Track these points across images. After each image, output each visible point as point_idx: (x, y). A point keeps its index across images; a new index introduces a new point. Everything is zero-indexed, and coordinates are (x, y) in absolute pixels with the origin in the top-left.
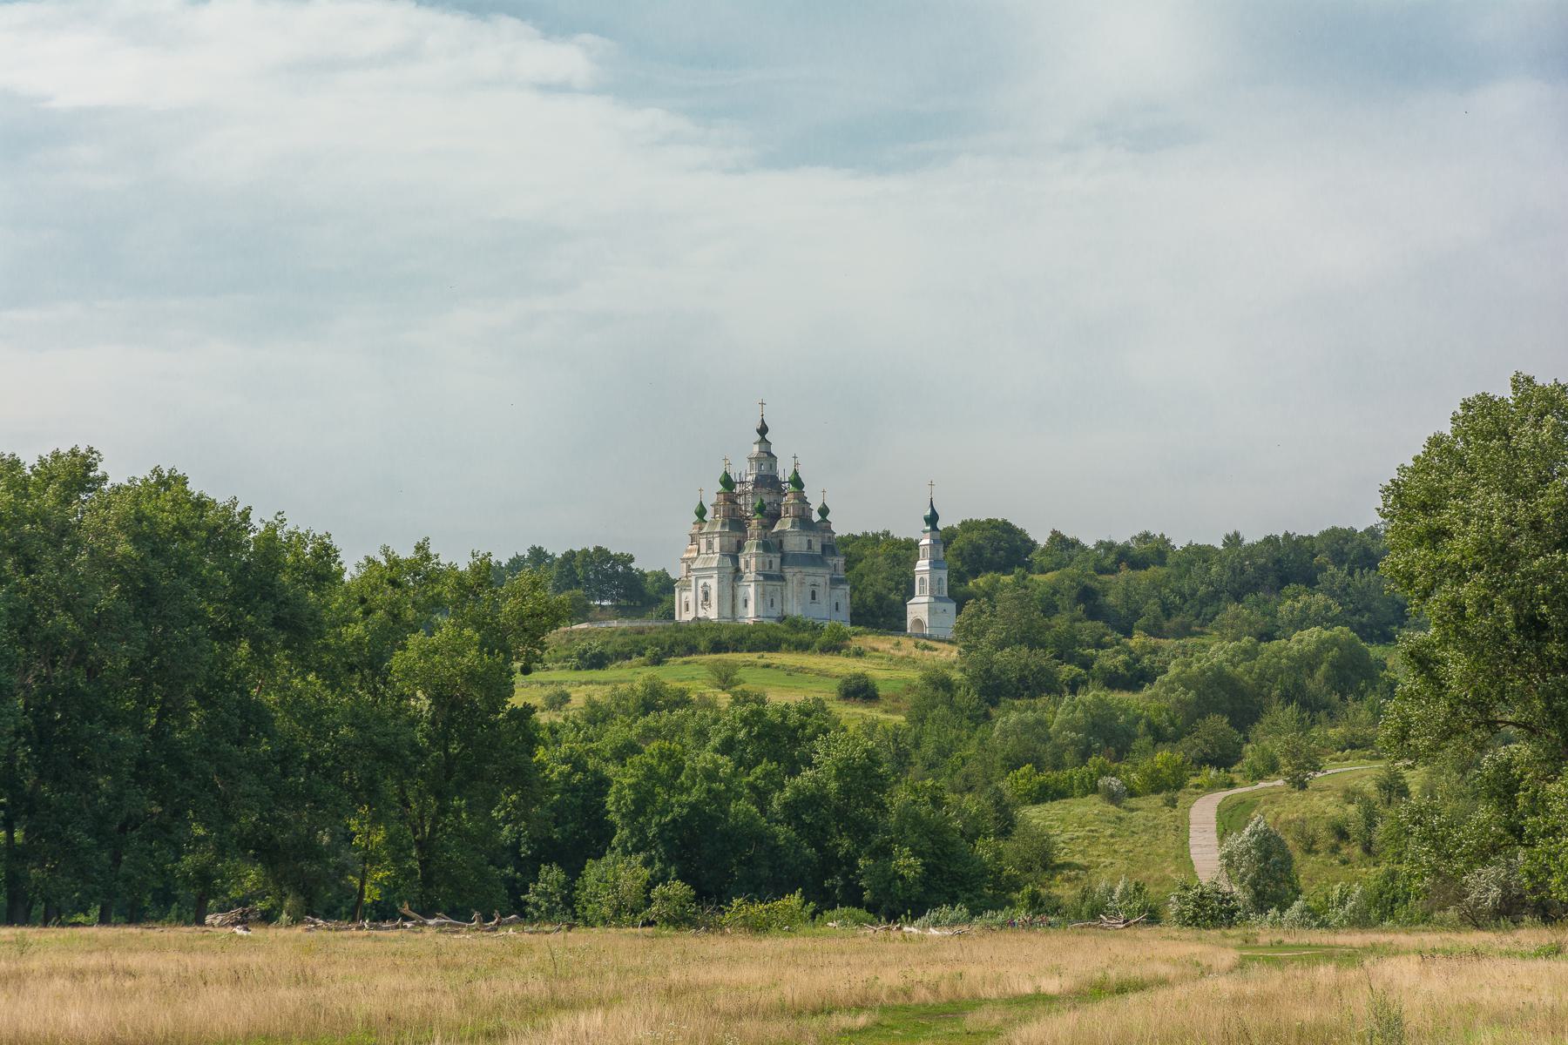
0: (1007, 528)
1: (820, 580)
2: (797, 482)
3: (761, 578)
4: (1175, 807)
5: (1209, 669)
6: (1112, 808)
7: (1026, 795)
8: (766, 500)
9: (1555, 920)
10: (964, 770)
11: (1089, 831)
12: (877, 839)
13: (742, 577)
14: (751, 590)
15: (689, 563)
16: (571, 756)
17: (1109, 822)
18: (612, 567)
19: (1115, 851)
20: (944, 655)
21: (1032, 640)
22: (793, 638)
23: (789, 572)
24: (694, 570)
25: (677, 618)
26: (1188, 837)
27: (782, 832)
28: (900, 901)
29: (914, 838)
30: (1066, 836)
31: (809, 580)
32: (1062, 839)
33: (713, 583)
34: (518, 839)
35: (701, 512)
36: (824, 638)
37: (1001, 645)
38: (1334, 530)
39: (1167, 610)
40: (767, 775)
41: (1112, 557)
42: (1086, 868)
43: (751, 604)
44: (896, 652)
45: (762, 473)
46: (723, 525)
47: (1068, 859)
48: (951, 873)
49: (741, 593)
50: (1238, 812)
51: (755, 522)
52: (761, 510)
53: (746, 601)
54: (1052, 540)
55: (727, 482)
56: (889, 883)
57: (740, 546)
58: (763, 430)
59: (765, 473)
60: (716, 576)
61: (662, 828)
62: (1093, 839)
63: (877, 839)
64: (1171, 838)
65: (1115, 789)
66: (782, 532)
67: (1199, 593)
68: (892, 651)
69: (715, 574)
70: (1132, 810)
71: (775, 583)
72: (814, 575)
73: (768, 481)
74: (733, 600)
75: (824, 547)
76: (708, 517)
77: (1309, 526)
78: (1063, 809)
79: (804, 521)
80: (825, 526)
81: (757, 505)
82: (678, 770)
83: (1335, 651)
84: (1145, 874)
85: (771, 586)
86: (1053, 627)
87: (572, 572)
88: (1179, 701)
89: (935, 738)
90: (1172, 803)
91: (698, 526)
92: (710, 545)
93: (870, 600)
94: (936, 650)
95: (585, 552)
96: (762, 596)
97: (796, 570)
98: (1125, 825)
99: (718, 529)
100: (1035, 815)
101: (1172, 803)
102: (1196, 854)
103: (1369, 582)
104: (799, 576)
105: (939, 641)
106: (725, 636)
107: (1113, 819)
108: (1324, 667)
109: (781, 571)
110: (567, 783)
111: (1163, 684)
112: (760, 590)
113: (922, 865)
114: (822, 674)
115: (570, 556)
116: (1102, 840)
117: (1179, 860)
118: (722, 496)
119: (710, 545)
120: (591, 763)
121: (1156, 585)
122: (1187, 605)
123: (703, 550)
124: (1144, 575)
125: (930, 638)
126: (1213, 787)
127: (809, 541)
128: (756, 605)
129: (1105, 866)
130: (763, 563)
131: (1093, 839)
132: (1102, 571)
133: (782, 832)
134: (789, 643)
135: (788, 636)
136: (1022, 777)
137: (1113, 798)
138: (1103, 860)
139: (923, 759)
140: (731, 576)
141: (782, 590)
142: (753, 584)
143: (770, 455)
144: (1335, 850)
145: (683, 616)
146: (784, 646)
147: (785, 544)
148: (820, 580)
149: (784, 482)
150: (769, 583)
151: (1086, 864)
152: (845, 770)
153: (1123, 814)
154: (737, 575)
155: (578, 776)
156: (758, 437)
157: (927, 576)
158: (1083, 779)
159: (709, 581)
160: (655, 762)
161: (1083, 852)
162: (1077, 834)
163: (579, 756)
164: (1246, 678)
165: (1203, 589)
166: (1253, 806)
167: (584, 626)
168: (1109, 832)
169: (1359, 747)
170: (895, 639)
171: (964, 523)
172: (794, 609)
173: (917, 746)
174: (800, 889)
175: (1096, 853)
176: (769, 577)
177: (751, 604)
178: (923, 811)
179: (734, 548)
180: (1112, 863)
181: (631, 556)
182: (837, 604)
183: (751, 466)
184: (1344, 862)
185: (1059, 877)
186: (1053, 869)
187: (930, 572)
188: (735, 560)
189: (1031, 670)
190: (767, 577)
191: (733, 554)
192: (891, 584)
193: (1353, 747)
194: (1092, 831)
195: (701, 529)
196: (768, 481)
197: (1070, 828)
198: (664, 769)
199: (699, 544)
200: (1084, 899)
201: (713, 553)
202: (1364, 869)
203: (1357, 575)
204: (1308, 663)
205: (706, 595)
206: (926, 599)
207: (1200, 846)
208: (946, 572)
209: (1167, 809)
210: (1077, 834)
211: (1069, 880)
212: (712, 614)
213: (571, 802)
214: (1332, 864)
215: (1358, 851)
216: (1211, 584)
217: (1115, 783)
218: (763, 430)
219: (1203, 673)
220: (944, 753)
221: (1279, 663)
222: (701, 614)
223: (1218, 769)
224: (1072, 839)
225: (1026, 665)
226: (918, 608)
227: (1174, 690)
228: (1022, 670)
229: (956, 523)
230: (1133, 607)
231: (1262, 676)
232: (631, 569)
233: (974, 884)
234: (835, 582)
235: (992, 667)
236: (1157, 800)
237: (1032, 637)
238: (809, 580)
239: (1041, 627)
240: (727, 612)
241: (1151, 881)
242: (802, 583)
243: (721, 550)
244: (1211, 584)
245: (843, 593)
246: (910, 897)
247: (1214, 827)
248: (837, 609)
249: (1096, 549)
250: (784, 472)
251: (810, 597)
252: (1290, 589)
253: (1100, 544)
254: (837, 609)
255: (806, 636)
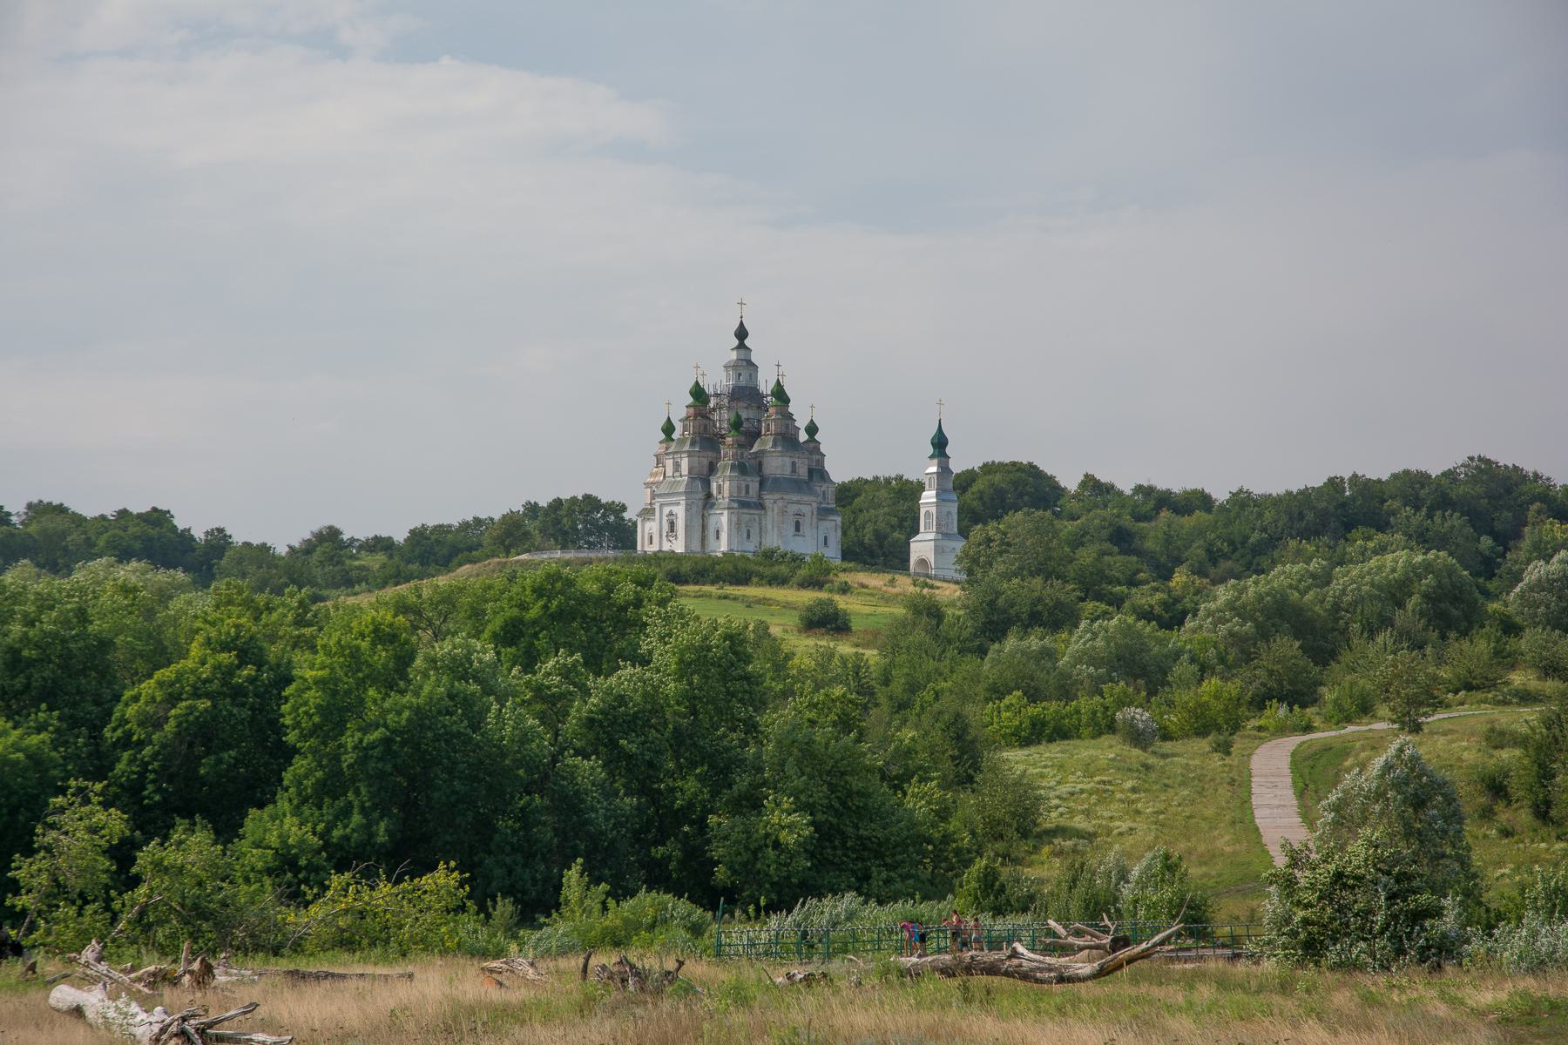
0: (1032, 471)
1: (805, 509)
2: (780, 394)
3: (736, 505)
4: (1228, 754)
5: (1268, 594)
6: (1136, 752)
7: (1012, 734)
8: (744, 415)
9: (860, 895)
10: (937, 706)
11: (1099, 783)
12: (742, 782)
13: (714, 504)
14: (724, 519)
15: (654, 488)
16: (237, 637)
17: (1130, 770)
18: (604, 515)
19: (1138, 812)
20: (947, 593)
21: (1045, 571)
22: (767, 571)
23: (769, 499)
24: (660, 495)
25: (639, 548)
26: (1250, 794)
27: (588, 770)
28: (773, 884)
29: (799, 782)
30: (1064, 789)
31: (793, 508)
32: (1057, 793)
33: (680, 511)
34: (142, 775)
35: (668, 429)
36: (803, 572)
37: (1007, 576)
38: (1407, 472)
39: (1214, 556)
40: (566, 673)
41: (1152, 503)
42: (1090, 836)
43: (724, 536)
44: (890, 589)
45: (740, 384)
46: (693, 443)
47: (1063, 822)
48: (860, 838)
49: (712, 521)
50: (1323, 761)
51: (729, 440)
52: (736, 425)
53: (718, 531)
54: (1083, 485)
55: (698, 393)
56: (755, 853)
57: (712, 468)
58: (742, 334)
59: (744, 384)
60: (683, 502)
61: (364, 751)
62: (1104, 795)
63: (742, 782)
64: (1224, 791)
65: (1141, 726)
66: (762, 452)
67: (1250, 541)
68: (884, 588)
69: (682, 500)
70: (1165, 756)
71: (752, 512)
72: (798, 502)
73: (745, 394)
74: (703, 531)
75: (811, 471)
76: (675, 436)
77: (1379, 470)
78: (1062, 752)
79: (787, 438)
80: (813, 447)
81: (732, 420)
82: (404, 660)
83: (1429, 580)
84: (1182, 846)
85: (746, 515)
86: (1077, 560)
87: (557, 522)
88: (1231, 634)
89: (906, 670)
90: (1225, 749)
91: (664, 445)
92: (677, 466)
93: (868, 538)
94: (938, 588)
95: (574, 500)
96: (736, 526)
97: (777, 496)
98: (1154, 776)
99: (687, 448)
100: (1017, 760)
101: (1225, 749)
102: (1262, 818)
103: (1453, 527)
104: (780, 503)
105: (945, 580)
106: (686, 568)
107: (1136, 766)
108: (1416, 599)
109: (760, 497)
110: (225, 683)
111: (1209, 614)
112: (734, 519)
113: (812, 823)
114: (788, 606)
115: (557, 504)
116: (1118, 796)
117: (1238, 826)
118: (692, 410)
119: (677, 466)
120: (273, 651)
121: (1200, 532)
122: (1237, 554)
123: (669, 472)
124: (1188, 522)
125: (936, 578)
126: (1282, 730)
127: (794, 464)
128: (729, 536)
129: (1121, 834)
130: (739, 488)
131: (1104, 795)
132: (1139, 518)
133: (588, 770)
134: (761, 577)
135: (761, 569)
136: (1008, 708)
137: (1138, 738)
138: (1117, 823)
139: (891, 698)
140: (701, 503)
141: (760, 519)
142: (726, 512)
143: (750, 363)
144: (1487, 814)
145: (645, 545)
146: (755, 580)
147: (764, 466)
148: (805, 509)
149: (767, 395)
150: (746, 511)
151: (1091, 830)
152: (695, 661)
153: (1152, 760)
154: (708, 501)
155: (249, 670)
156: (736, 342)
157: (933, 510)
158: (1094, 713)
159: (675, 509)
160: (364, 645)
161: (1087, 813)
162: (1080, 786)
163: (251, 638)
164: (1317, 608)
165: (1255, 537)
166: (1345, 753)
167: (524, 557)
168: (1129, 784)
169: (1477, 688)
170: (888, 577)
171: (985, 465)
172: (772, 541)
173: (886, 682)
174: (580, 860)
175: (1107, 814)
176: (746, 505)
177: (724, 536)
178: (819, 736)
179: (705, 471)
180: (1131, 829)
181: (624, 505)
182: (826, 537)
183: (728, 375)
184: (1506, 833)
185: (1046, 849)
186: (1039, 836)
187: (938, 504)
188: (707, 484)
189: (1046, 605)
190: (744, 505)
191: (703, 477)
192: (894, 521)
193: (1469, 687)
194: (1104, 783)
195: (667, 449)
196: (745, 394)
197: (1071, 778)
198: (382, 656)
199: (664, 466)
200: (1074, 882)
201: (681, 476)
202: (1543, 845)
203: (1438, 519)
204: (1396, 593)
205: (672, 525)
206: (932, 536)
207: (1269, 806)
208: (956, 505)
209: (1216, 756)
210: (1080, 786)
211: (1059, 853)
212: (679, 547)
213: (231, 714)
214: (1485, 836)
215: (1524, 817)
216: (1264, 530)
217: (1139, 715)
218: (742, 334)
219: (1260, 598)
220: (913, 688)
221: (1359, 589)
222: (666, 547)
223: (1291, 706)
224: (1072, 794)
225: (1040, 600)
226: (922, 547)
227: (1224, 621)
228: (1033, 604)
229: (975, 464)
230: (1175, 553)
231: (1337, 607)
232: (623, 519)
233: (899, 857)
234: (824, 513)
235: (997, 598)
236: (1204, 744)
237: (1050, 569)
238: (793, 508)
239: (1061, 559)
240: (696, 547)
241: (1193, 858)
242: (783, 512)
243: (690, 472)
244: (1264, 530)
245: (833, 527)
246: (788, 878)
247: (1289, 780)
248: (826, 544)
249: (1134, 495)
250: (766, 385)
251: (793, 529)
252: (1354, 533)
253: (1139, 489)
254: (826, 544)
255: (784, 569)
